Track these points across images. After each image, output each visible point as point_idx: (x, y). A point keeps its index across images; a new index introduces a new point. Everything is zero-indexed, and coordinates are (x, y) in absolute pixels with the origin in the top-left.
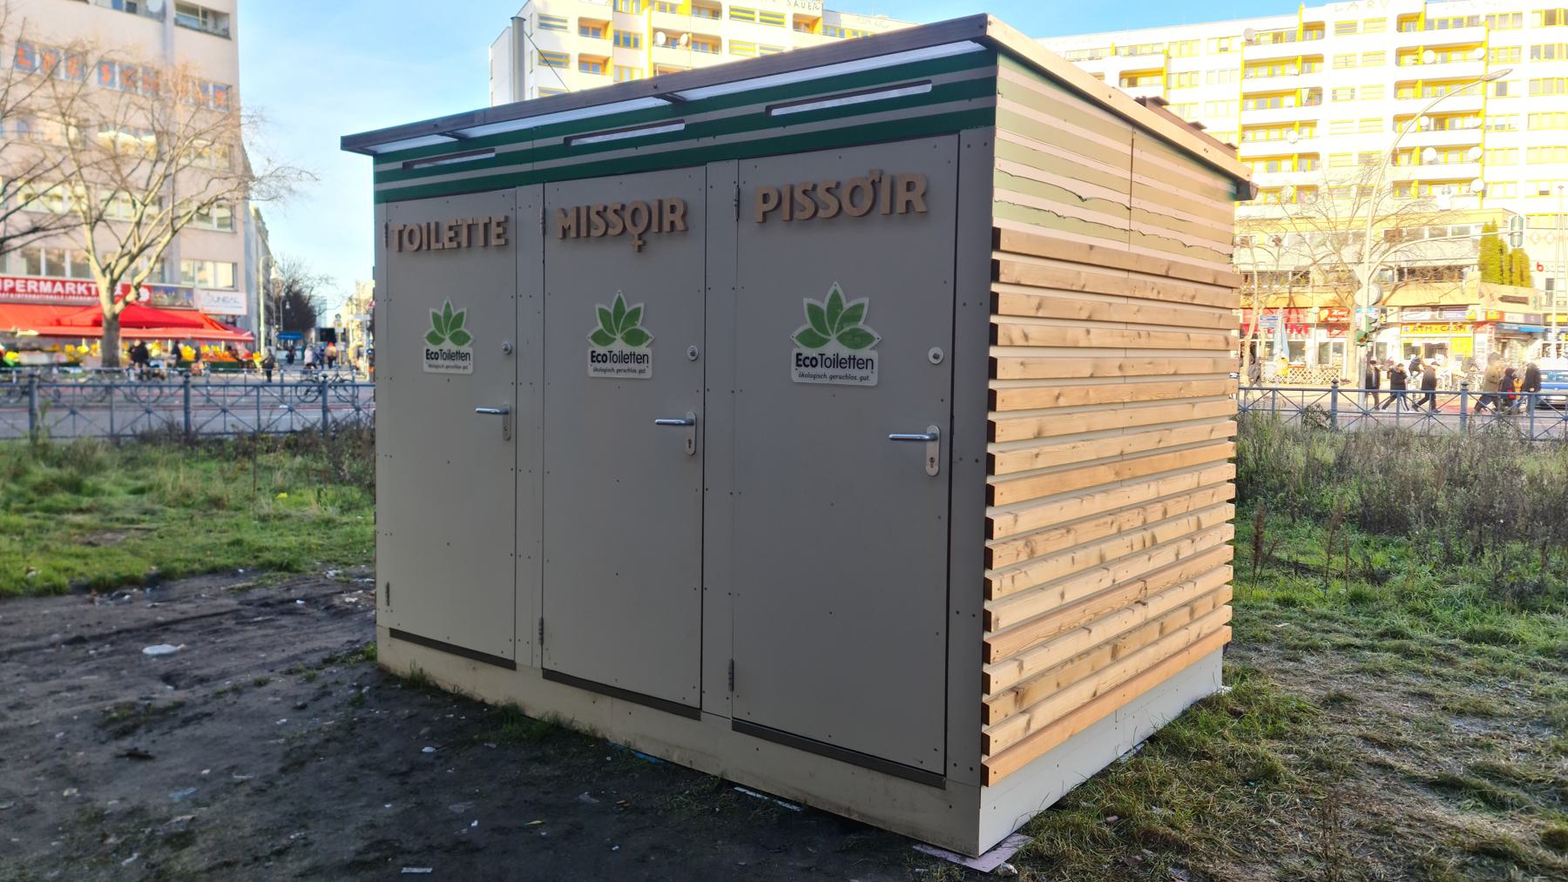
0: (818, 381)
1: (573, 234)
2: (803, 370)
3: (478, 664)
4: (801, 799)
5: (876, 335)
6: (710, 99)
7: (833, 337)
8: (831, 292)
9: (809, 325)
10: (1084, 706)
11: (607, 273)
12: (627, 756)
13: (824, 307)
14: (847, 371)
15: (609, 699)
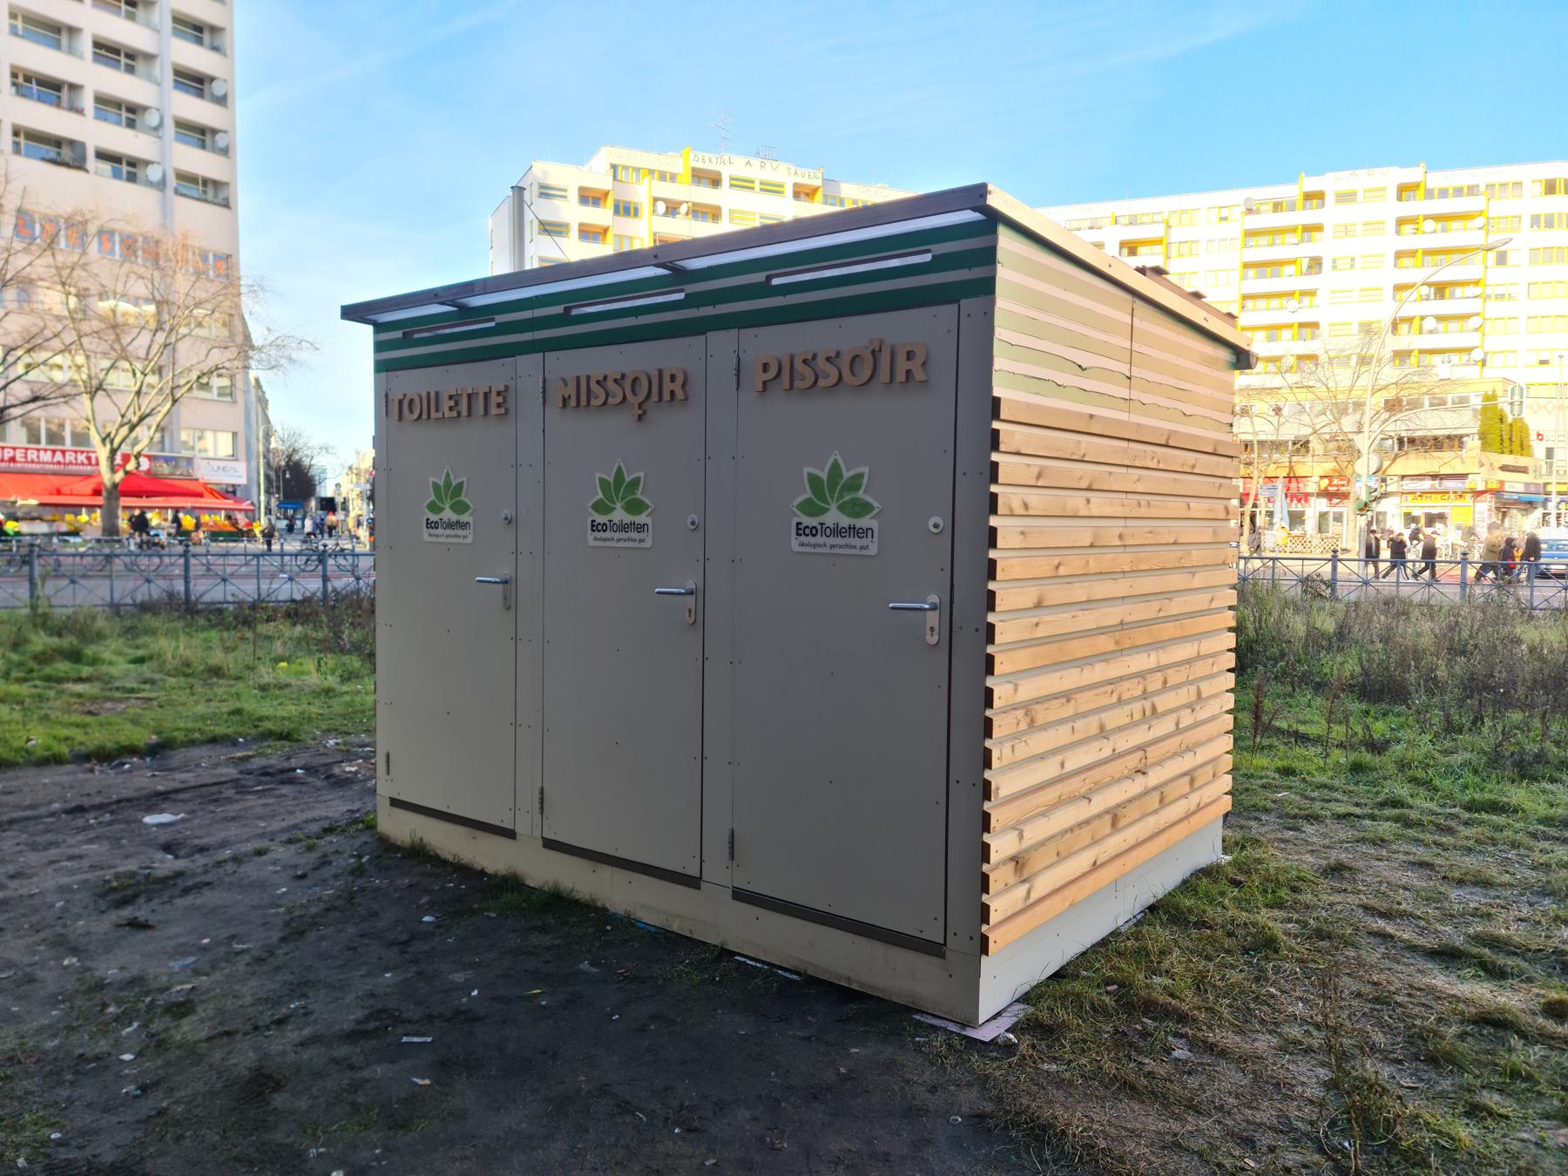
4: (801, 968)
5: (876, 504)
6: (522, 310)
7: (833, 506)
8: (831, 461)
9: (809, 494)
11: (607, 443)
12: (627, 924)
15: (609, 868)
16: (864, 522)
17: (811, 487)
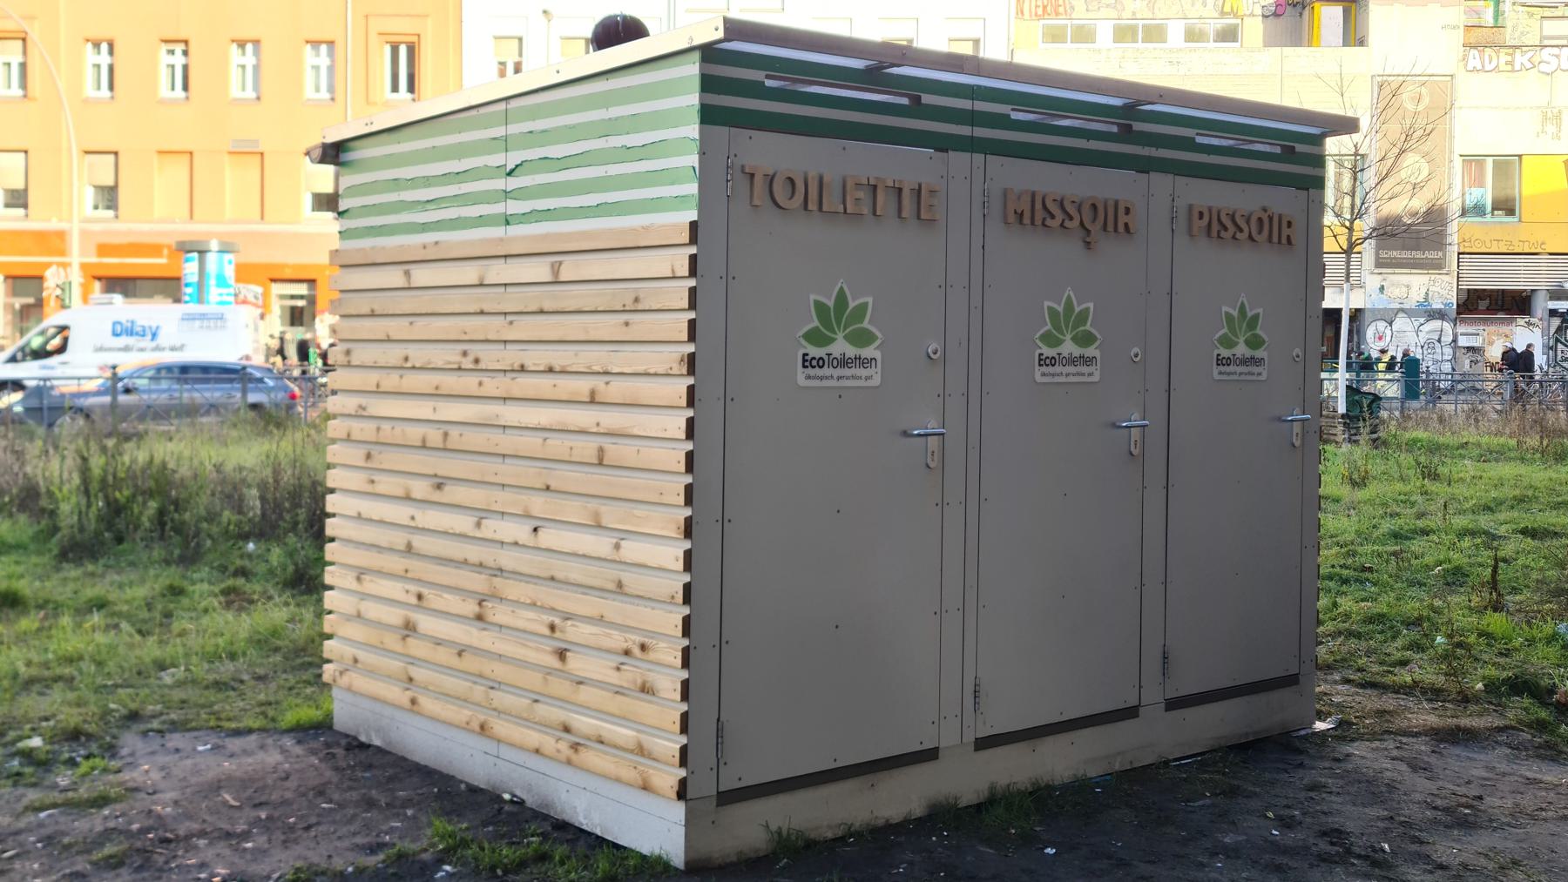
0: (1057, 379)
1: (1027, 220)
2: (810, 371)
3: (870, 778)
5: (878, 334)
10: (450, 724)
12: (1079, 788)
13: (831, 303)
14: (1250, 369)
17: (819, 316)
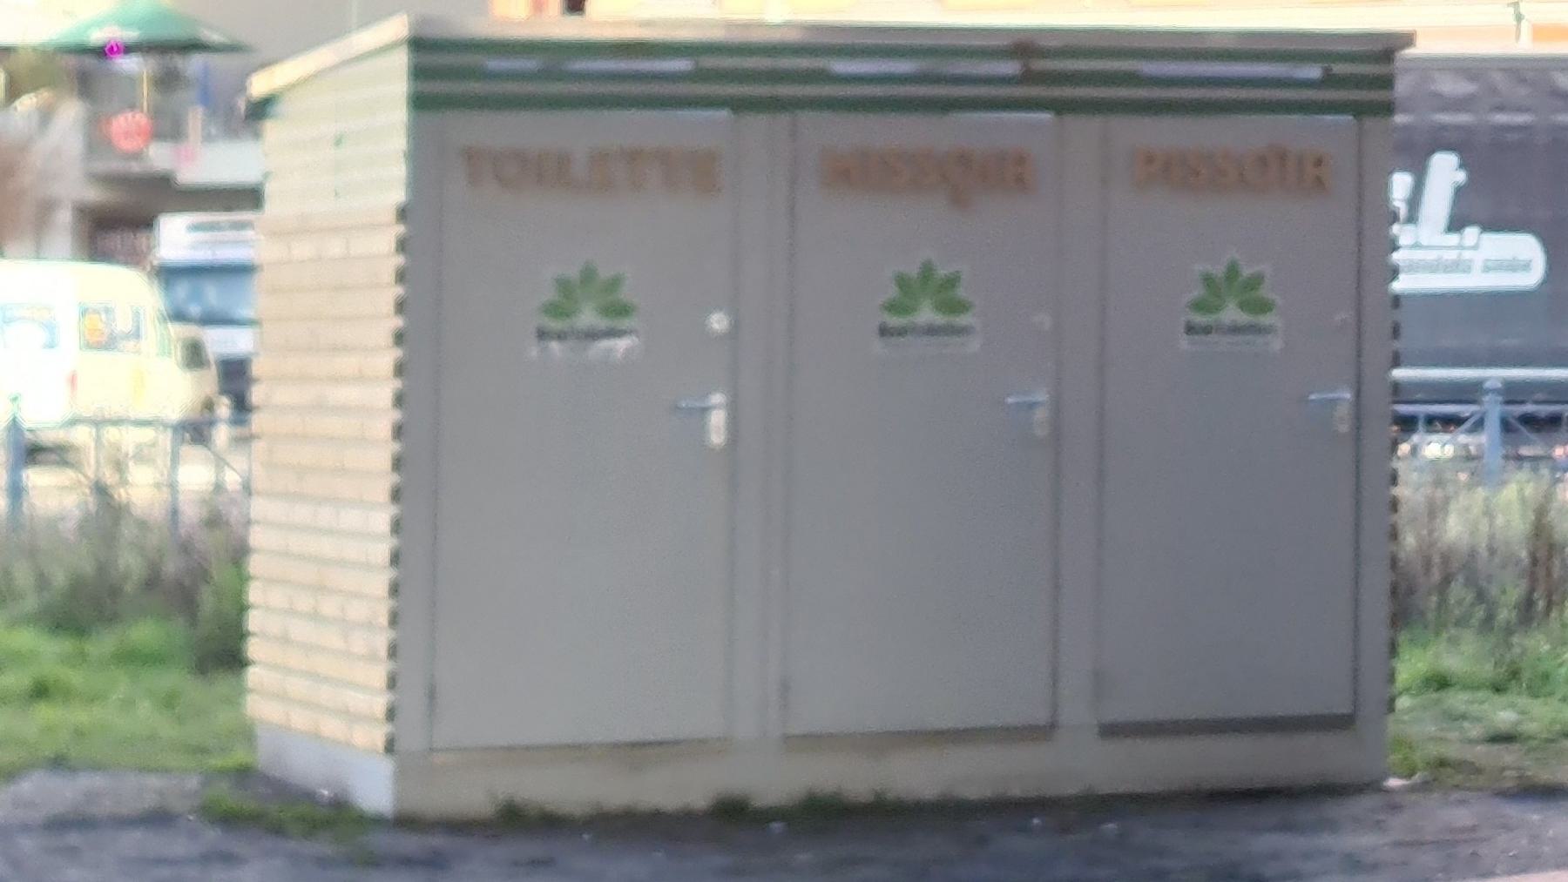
5: (1279, 301)
11: (911, 233)
16: (963, 320)
